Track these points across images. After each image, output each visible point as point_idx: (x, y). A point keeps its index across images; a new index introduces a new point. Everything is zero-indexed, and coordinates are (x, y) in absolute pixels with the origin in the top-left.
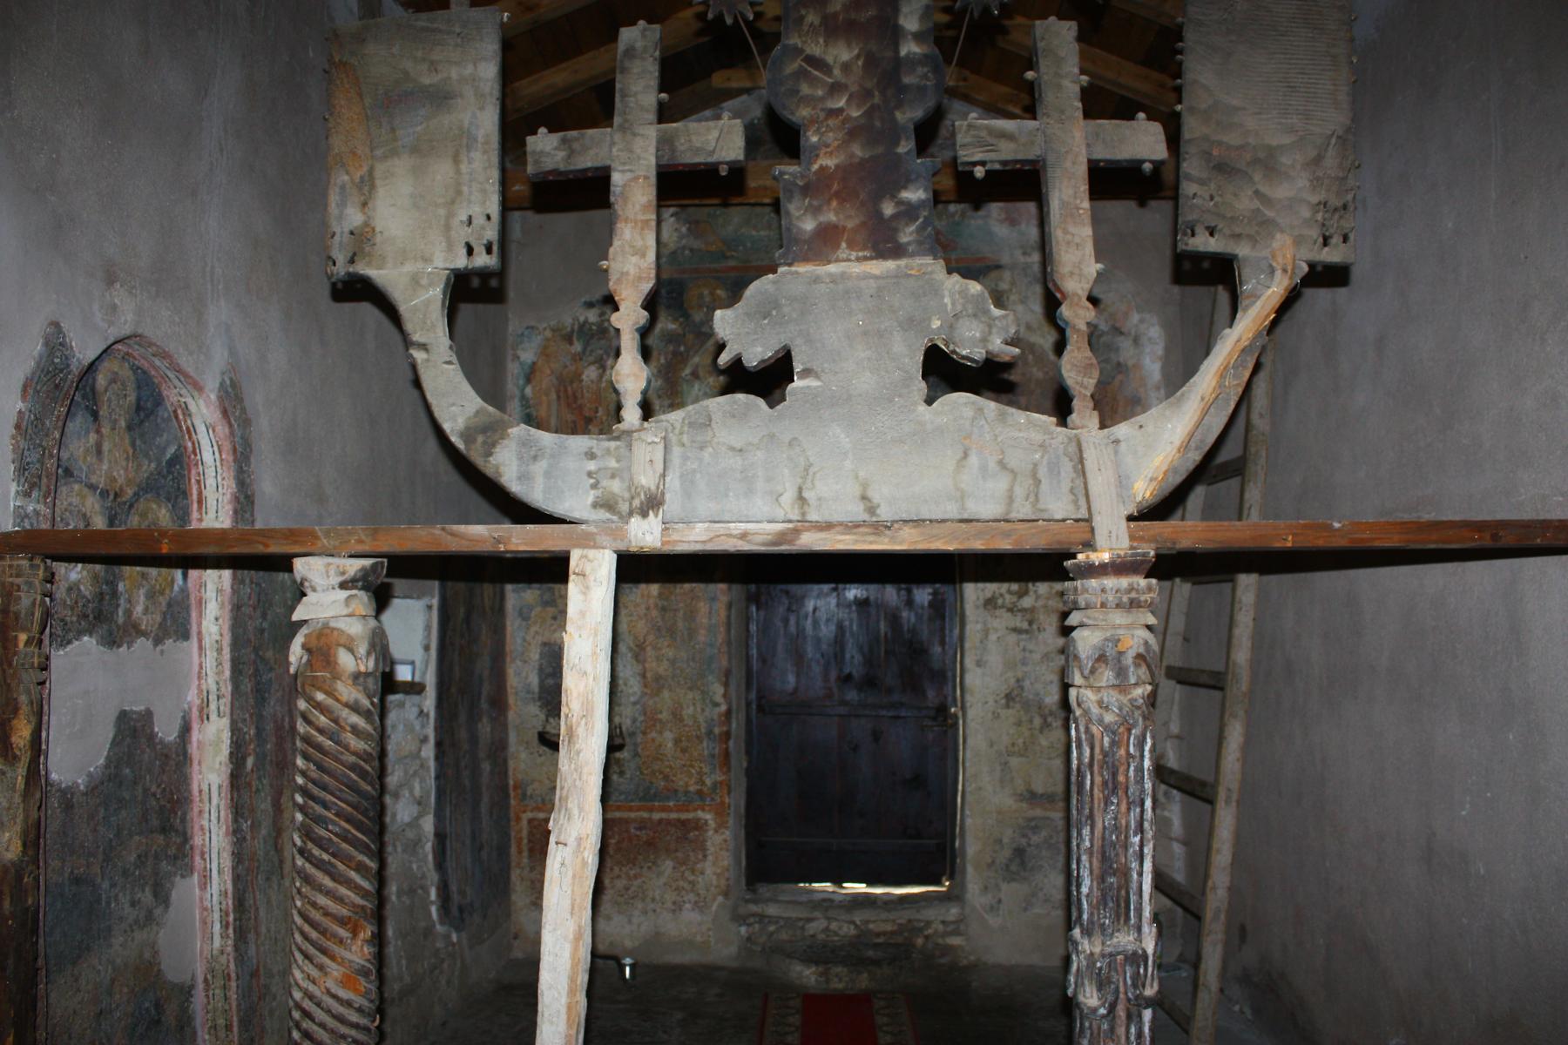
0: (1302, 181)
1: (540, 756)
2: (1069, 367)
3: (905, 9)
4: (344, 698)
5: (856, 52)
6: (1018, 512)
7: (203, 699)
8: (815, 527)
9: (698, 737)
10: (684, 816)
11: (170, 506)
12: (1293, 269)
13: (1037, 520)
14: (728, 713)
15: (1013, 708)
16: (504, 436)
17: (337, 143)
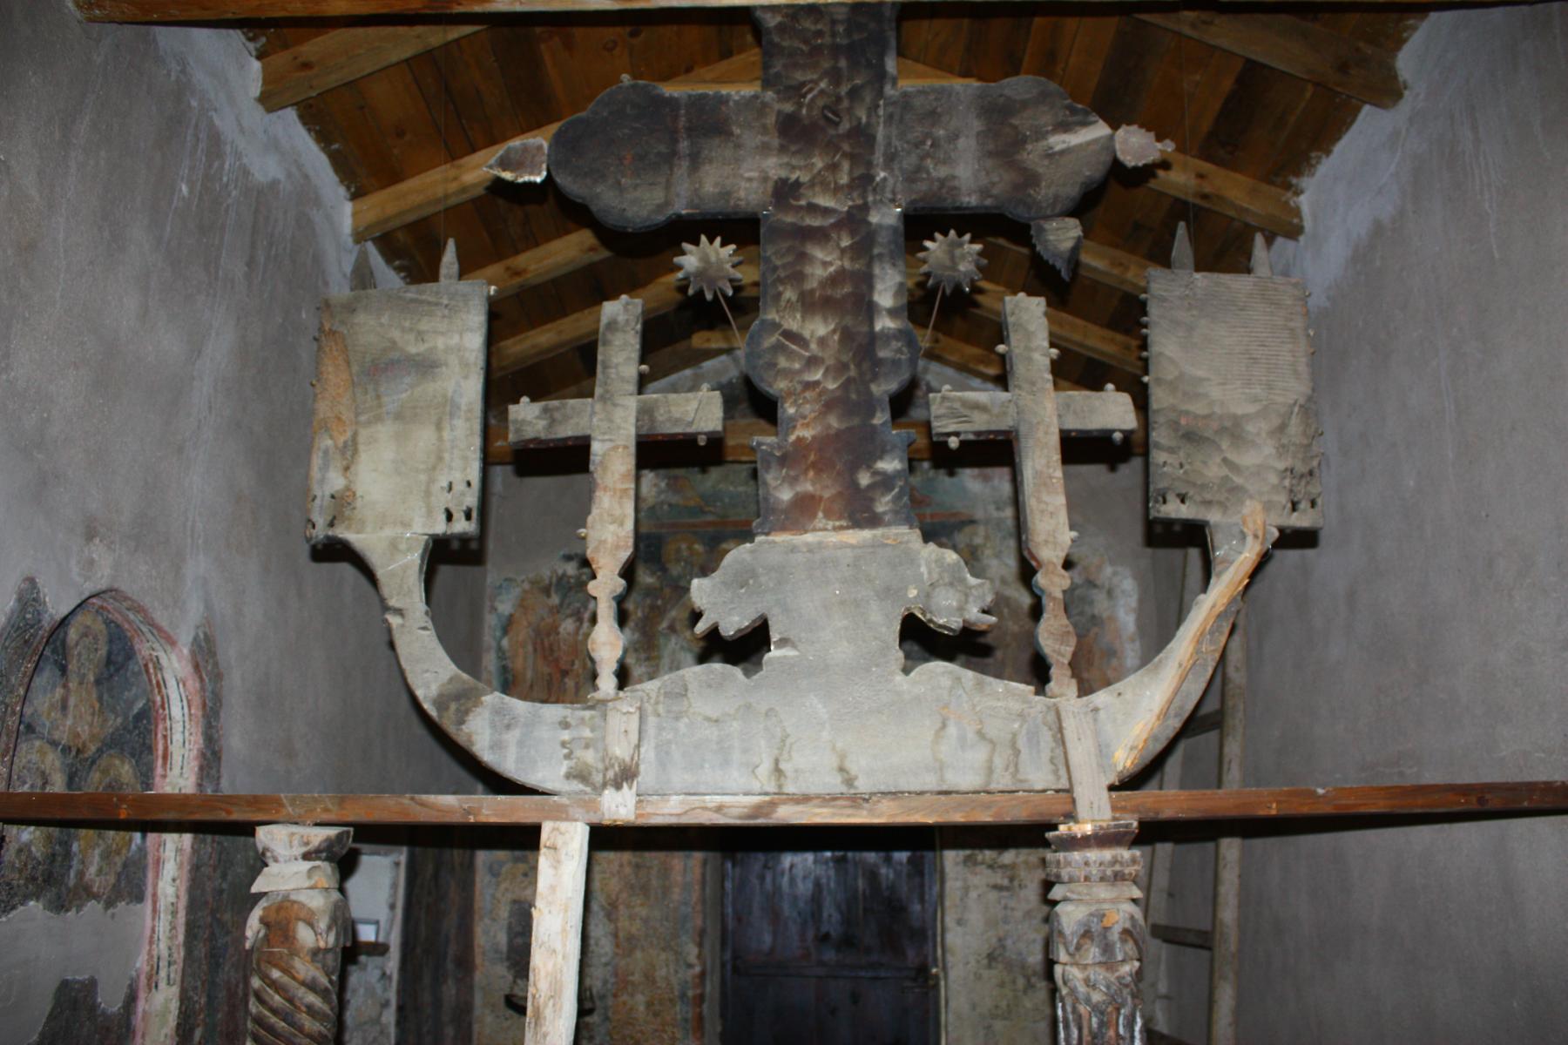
0: (1269, 449)
1: (507, 1019)
2: (1046, 635)
3: (879, 286)
4: (301, 976)
5: (832, 327)
6: (998, 783)
7: (152, 966)
8: (791, 800)
11: (134, 762)
12: (1264, 535)
13: (1017, 791)
14: (703, 975)
16: (477, 703)
17: (323, 408)
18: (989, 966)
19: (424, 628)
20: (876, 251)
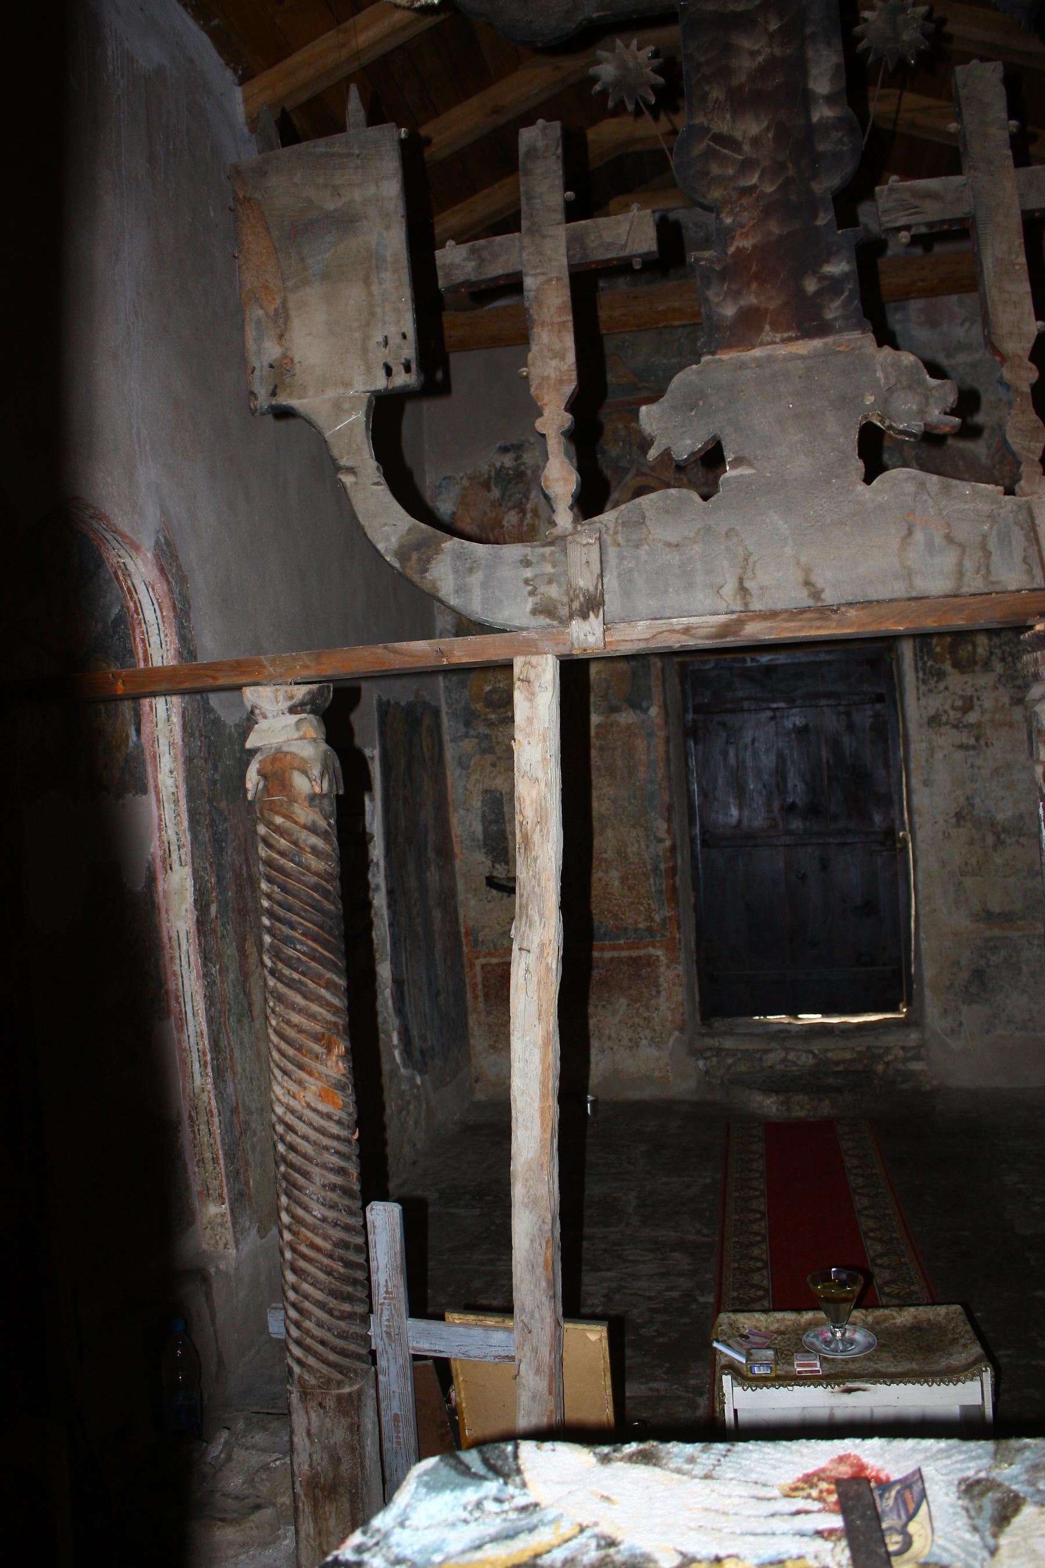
1: (489, 902)
3: (814, 71)
4: (302, 820)
5: (765, 123)
6: (970, 586)
9: (644, 874)
10: (635, 953)
13: (990, 593)
14: (673, 848)
15: (964, 826)
16: (438, 551)
18: (958, 825)
19: (377, 484)
20: (808, 31)
